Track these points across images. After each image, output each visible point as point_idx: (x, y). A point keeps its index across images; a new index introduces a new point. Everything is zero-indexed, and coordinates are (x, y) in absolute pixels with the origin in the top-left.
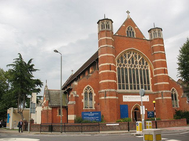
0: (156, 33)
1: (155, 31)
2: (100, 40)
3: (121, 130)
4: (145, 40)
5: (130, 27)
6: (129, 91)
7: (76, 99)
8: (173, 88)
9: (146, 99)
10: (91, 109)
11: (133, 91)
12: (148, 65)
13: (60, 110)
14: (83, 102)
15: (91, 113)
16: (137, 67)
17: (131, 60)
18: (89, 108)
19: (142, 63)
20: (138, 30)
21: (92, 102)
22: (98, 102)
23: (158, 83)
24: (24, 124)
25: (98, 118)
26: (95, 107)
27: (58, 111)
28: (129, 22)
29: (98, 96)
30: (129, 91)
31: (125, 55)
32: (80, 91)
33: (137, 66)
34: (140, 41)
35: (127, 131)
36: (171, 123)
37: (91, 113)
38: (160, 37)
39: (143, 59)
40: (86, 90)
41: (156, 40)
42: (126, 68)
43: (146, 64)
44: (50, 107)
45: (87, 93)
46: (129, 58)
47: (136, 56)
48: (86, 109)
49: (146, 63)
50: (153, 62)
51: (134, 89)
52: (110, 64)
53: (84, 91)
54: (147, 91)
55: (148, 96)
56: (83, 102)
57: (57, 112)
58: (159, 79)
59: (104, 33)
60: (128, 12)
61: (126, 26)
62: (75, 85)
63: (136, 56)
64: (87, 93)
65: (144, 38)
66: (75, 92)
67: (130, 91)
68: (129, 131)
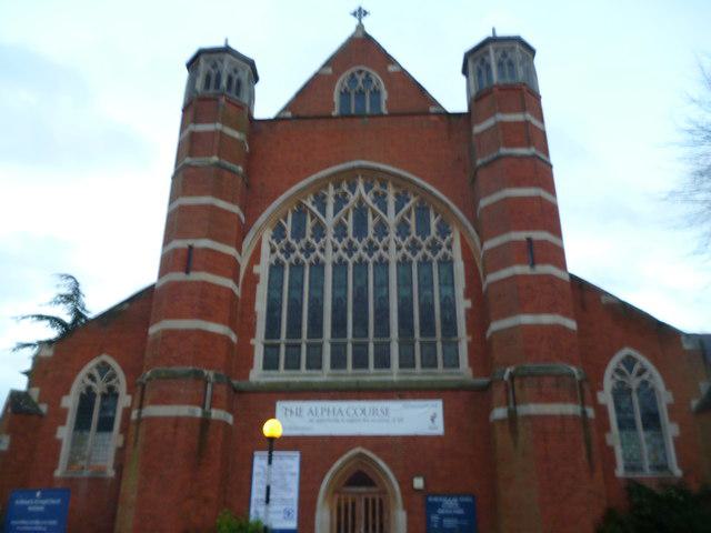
9: (421, 418)
12: (456, 236)
37: (38, 494)
40: (618, 377)
45: (629, 391)
53: (77, 388)
65: (432, 109)
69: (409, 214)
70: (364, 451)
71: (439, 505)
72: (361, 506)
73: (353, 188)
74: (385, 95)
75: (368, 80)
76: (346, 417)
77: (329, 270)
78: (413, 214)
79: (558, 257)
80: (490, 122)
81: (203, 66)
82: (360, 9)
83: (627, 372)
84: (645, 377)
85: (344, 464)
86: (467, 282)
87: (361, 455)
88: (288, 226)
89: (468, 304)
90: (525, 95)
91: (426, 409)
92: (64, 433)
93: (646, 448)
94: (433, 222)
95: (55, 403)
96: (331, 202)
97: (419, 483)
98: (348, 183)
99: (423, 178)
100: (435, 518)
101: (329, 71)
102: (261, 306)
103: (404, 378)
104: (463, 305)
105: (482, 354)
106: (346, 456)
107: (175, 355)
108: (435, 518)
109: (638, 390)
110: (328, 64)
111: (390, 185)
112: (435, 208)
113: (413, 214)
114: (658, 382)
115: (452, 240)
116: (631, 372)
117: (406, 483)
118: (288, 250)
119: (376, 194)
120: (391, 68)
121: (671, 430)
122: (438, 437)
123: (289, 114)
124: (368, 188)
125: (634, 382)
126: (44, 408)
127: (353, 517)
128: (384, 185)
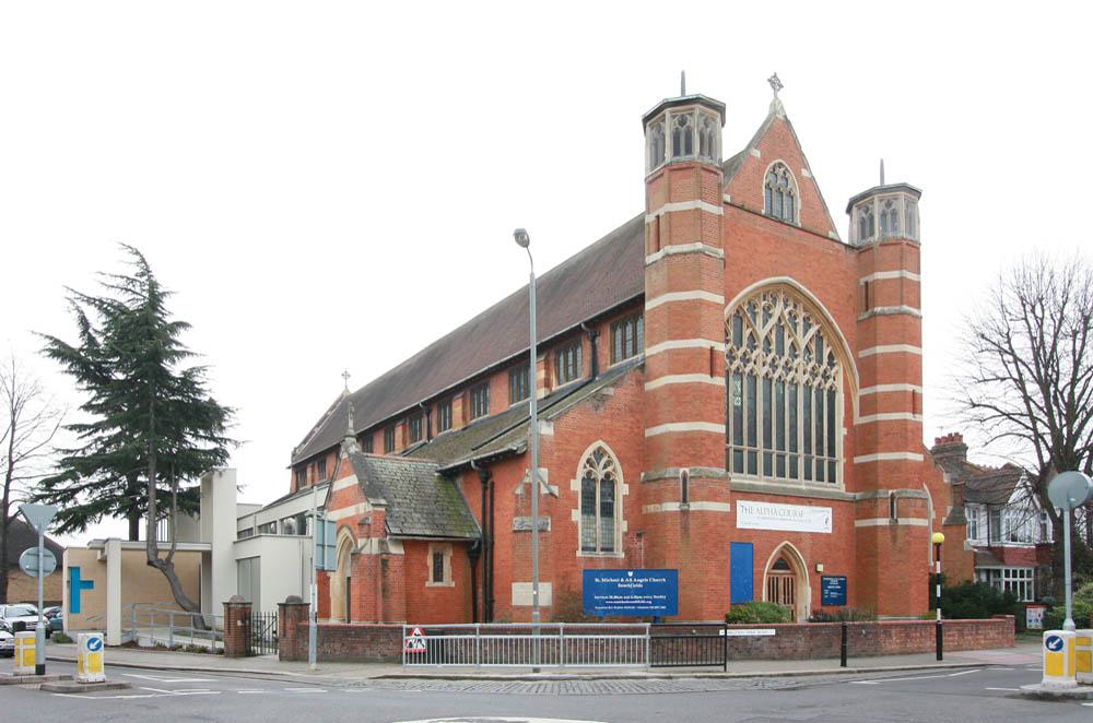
0: (894, 213)
1: (889, 204)
2: (661, 212)
3: (784, 657)
4: (832, 240)
5: (780, 165)
6: (760, 481)
7: (551, 505)
8: (600, 443)
9: (818, 520)
10: (609, 555)
11: (774, 482)
12: (838, 369)
13: (438, 559)
14: (577, 522)
15: (630, 574)
16: (752, 364)
17: (773, 337)
18: (601, 554)
19: (773, 347)
20: (811, 186)
21: (613, 525)
22: (644, 528)
23: (881, 456)
24: (239, 623)
25: (661, 602)
26: (627, 550)
27: (430, 561)
28: (778, 136)
29: (640, 497)
30: (760, 481)
31: (753, 307)
32: (563, 471)
33: (753, 356)
34: (819, 244)
35: (835, 666)
36: (966, 632)
37: (630, 574)
38: (707, 160)
39: (819, 338)
40: (589, 468)
41: (891, 248)
42: (752, 371)
43: (831, 364)
44: (396, 542)
45: (594, 480)
46: (768, 327)
47: (793, 317)
48: (588, 554)
49: (831, 357)
50: (863, 354)
51: (778, 476)
52: (713, 344)
53: (581, 473)
54: (825, 487)
55: (830, 509)
56: (577, 522)
57: (425, 565)
58: (887, 435)
59: (687, 181)
60: (775, 83)
61: (765, 160)
62: (542, 438)
63: (793, 317)
64: (594, 480)
65: (831, 235)
66: (544, 472)
67: (762, 483)
68: (844, 664)
74: (799, 205)
78: (774, 332)
80: (895, 274)
82: (769, 80)
84: (609, 469)
90: (907, 252)
91: (822, 514)
95: (565, 487)
96: (760, 311)
97: (820, 568)
99: (828, 308)
100: (826, 592)
104: (841, 432)
105: (862, 477)
107: (713, 456)
111: (800, 307)
112: (828, 340)
113: (774, 332)
119: (790, 313)
122: (828, 534)
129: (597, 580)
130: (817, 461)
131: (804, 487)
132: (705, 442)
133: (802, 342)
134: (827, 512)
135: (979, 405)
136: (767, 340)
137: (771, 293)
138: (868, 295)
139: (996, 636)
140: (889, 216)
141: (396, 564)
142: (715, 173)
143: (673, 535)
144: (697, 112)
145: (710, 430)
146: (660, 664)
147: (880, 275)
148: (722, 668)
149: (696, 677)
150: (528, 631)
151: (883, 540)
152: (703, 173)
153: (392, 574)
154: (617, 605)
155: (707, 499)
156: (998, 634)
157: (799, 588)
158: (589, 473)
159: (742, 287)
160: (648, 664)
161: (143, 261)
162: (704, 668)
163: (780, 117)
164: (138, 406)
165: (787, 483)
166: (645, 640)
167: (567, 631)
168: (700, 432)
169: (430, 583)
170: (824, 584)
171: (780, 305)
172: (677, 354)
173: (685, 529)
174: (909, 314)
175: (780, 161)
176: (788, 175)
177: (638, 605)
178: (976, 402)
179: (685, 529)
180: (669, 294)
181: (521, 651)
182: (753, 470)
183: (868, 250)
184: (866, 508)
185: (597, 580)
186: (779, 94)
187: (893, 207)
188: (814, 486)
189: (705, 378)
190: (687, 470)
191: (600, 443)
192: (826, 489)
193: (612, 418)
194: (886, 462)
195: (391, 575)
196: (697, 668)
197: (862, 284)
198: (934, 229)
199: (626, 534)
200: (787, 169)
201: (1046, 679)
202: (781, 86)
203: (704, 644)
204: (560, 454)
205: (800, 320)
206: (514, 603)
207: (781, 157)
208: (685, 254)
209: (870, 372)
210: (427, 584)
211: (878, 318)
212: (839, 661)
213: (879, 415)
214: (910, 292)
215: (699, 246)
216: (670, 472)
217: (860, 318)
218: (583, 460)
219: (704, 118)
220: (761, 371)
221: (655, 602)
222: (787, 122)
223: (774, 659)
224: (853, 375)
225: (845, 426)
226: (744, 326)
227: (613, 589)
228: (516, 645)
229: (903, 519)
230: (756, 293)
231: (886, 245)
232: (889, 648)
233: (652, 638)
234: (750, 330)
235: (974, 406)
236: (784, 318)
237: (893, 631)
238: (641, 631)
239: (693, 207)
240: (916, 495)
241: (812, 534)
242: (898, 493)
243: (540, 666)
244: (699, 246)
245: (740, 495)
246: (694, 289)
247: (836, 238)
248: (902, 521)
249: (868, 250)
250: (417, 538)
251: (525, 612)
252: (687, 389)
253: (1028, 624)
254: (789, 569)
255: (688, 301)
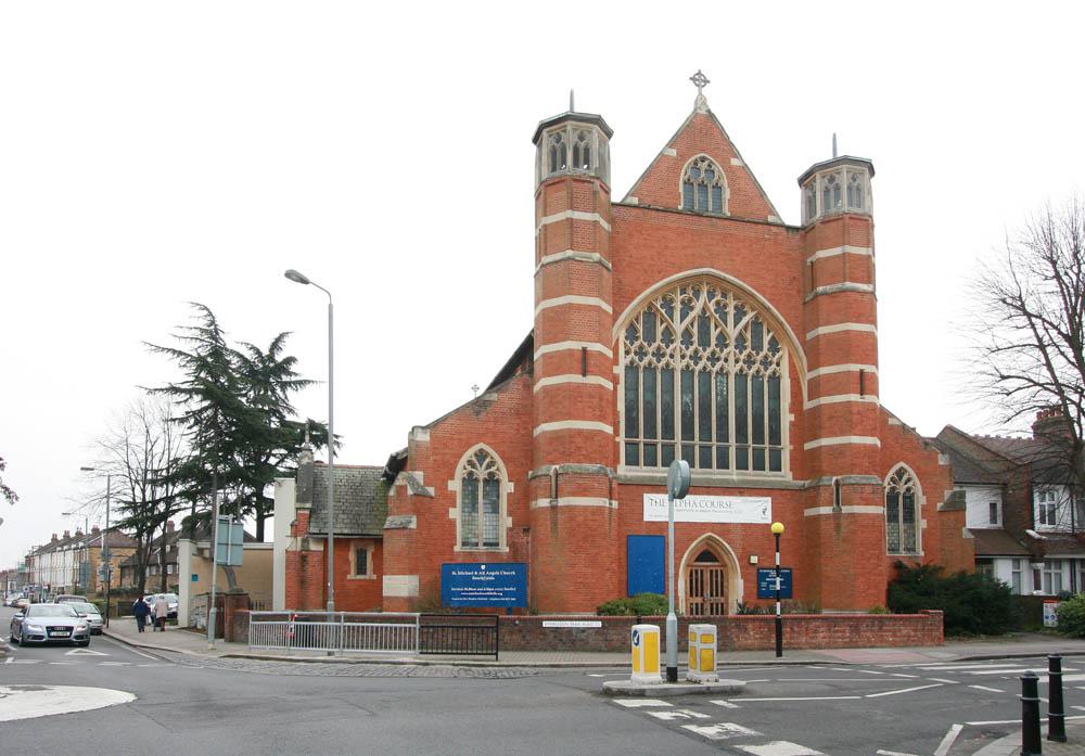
0: (838, 188)
9: (754, 511)
10: (492, 549)
12: (784, 353)
17: (695, 330)
18: (482, 548)
22: (525, 522)
26: (511, 545)
35: (771, 656)
37: (483, 567)
39: (756, 325)
40: (469, 468)
41: (833, 224)
45: (477, 480)
46: (687, 320)
47: (721, 308)
48: (467, 549)
52: (584, 344)
54: (767, 476)
55: (769, 499)
58: (831, 417)
60: (699, 80)
63: (721, 308)
65: (771, 219)
68: (779, 654)
69: (692, 324)
70: (713, 535)
71: (767, 575)
72: (707, 576)
73: (697, 294)
74: (727, 194)
75: (710, 171)
76: (699, 509)
77: (678, 376)
78: (696, 325)
79: (866, 383)
80: (837, 251)
81: (820, 184)
83: (478, 465)
85: (696, 546)
86: (792, 397)
87: (709, 538)
88: (640, 328)
89: (791, 417)
90: (863, 226)
92: (455, 513)
93: (902, 535)
94: (767, 338)
95: (442, 488)
96: (678, 306)
97: (754, 559)
98: (693, 288)
101: (673, 153)
102: (621, 407)
103: (741, 477)
104: (787, 418)
105: (807, 464)
106: (700, 539)
108: (764, 584)
109: (485, 481)
110: (672, 144)
111: (731, 295)
113: (696, 325)
114: (918, 490)
115: (781, 358)
116: (481, 466)
117: (745, 558)
118: (641, 353)
119: (718, 303)
120: (734, 162)
121: (922, 524)
123: (635, 201)
124: (711, 295)
125: (902, 489)
126: (431, 491)
127: (702, 582)
128: (724, 295)
129: (454, 573)
130: (683, 446)
131: (735, 477)
132: (574, 440)
133: (732, 332)
134: (766, 502)
135: (1009, 377)
136: (687, 334)
137: (692, 285)
138: (812, 274)
139: (912, 634)
140: (832, 193)
141: (315, 559)
142: (589, 182)
143: (543, 528)
144: (569, 128)
145: (581, 427)
146: (430, 651)
147: (821, 254)
148: (494, 657)
149: (453, 665)
150: (323, 618)
151: (827, 529)
152: (574, 184)
153: (310, 569)
154: (472, 596)
155: (574, 494)
156: (915, 631)
157: (730, 581)
158: (471, 474)
159: (648, 284)
160: (418, 651)
161: (210, 314)
162: (477, 657)
163: (703, 112)
164: (233, 428)
165: (715, 474)
166: (415, 628)
167: (348, 619)
168: (569, 430)
169: (352, 576)
170: (761, 577)
171: (704, 296)
172: (551, 358)
173: (555, 523)
174: (853, 291)
175: (703, 155)
176: (713, 167)
177: (491, 596)
178: (1005, 374)
179: (555, 523)
180: (546, 301)
181: (367, 636)
182: (724, 464)
183: (813, 228)
184: (811, 496)
185: (454, 573)
186: (705, 91)
187: (836, 182)
188: (751, 475)
189: (577, 378)
190: (558, 467)
191: (481, 445)
192: (767, 478)
193: (495, 422)
194: (830, 447)
195: (309, 569)
196: (456, 656)
197: (809, 264)
198: (886, 202)
199: (510, 530)
200: (711, 162)
201: (635, 675)
202: (707, 82)
203: (455, 633)
204: (437, 458)
205: (731, 311)
206: (384, 595)
207: (703, 151)
208: (556, 262)
209: (816, 353)
210: (349, 577)
211: (820, 298)
212: (774, 653)
213: (822, 399)
214: (865, 269)
215: (570, 253)
216: (543, 470)
217: (807, 299)
218: (463, 461)
219: (578, 132)
220: (678, 365)
221: (506, 594)
222: (711, 115)
223: (600, 651)
224: (801, 360)
225: (792, 411)
226: (658, 322)
227: (468, 581)
228: (363, 632)
229: (848, 507)
230: (671, 287)
231: (829, 221)
232: (743, 642)
233: (422, 627)
234: (664, 325)
235: (1004, 377)
236: (709, 309)
237: (750, 626)
238: (412, 620)
239: (564, 218)
240: (864, 481)
241: (742, 524)
242: (843, 479)
243: (334, 650)
244: (570, 253)
245: (646, 488)
246: (564, 294)
247: (779, 222)
248: (845, 509)
249: (813, 228)
250: (1076, 518)
251: (396, 602)
252: (559, 389)
253: (1045, 620)
254: (717, 561)
255: (559, 306)
